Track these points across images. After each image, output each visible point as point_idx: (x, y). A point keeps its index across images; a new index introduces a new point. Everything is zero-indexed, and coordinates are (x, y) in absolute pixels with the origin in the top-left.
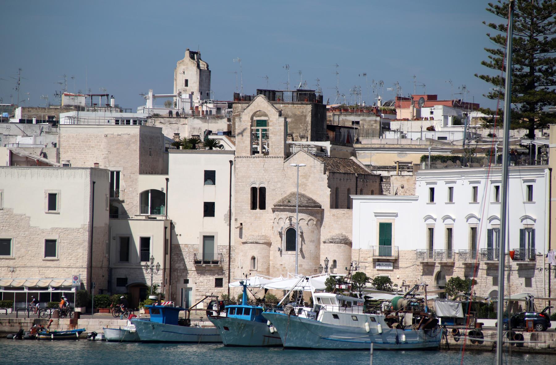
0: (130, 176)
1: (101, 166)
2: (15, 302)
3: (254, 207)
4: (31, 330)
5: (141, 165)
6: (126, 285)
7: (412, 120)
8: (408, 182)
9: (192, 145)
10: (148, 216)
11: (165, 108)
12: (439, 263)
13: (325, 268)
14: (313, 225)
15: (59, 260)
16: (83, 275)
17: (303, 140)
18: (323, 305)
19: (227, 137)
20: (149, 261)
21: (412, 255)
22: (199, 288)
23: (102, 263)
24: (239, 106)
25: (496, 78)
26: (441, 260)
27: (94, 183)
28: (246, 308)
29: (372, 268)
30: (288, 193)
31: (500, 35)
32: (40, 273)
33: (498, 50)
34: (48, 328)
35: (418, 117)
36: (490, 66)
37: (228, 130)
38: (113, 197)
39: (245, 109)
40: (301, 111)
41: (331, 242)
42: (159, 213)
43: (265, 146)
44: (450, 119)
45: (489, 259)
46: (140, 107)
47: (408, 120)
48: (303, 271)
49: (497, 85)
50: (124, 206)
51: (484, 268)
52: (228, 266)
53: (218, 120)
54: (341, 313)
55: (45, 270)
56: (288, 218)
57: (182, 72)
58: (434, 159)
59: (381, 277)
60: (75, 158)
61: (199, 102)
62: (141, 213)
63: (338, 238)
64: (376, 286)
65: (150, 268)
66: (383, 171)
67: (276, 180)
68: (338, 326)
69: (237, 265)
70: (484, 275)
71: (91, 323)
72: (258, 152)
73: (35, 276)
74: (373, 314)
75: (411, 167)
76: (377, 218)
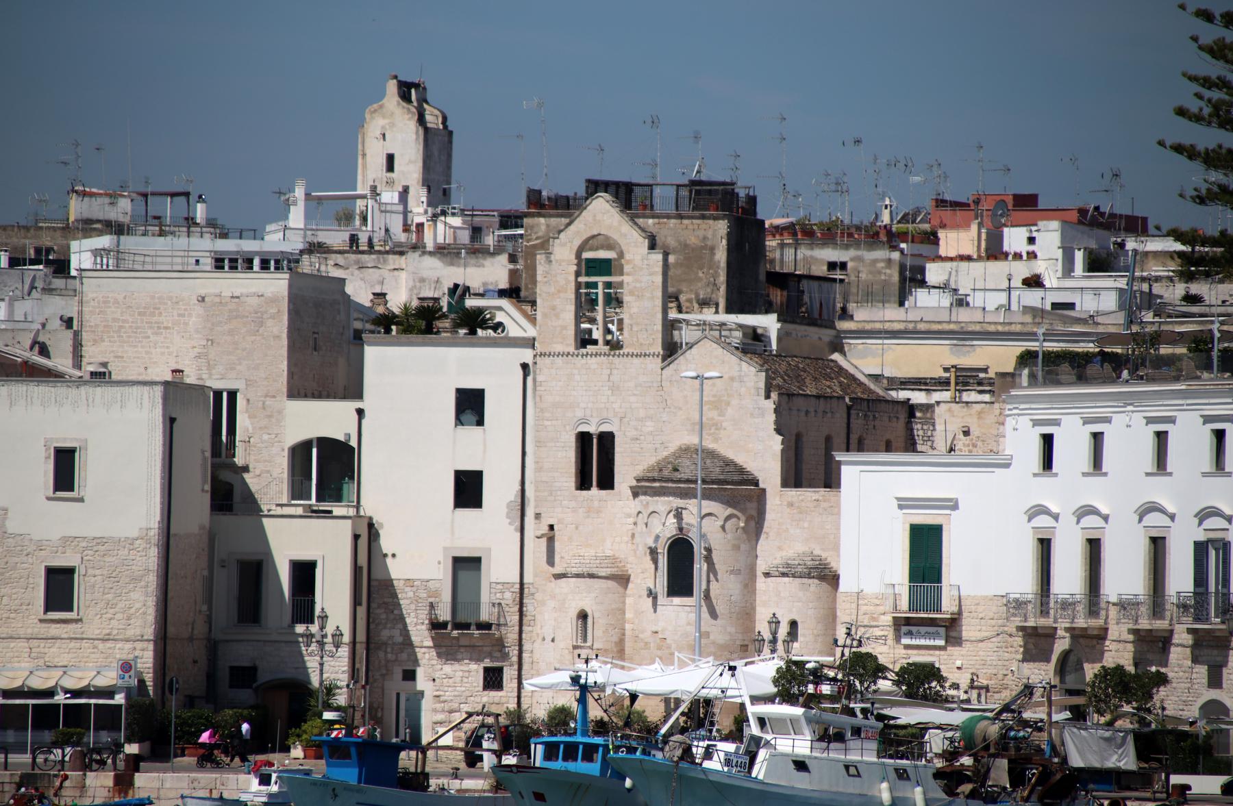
0: (264, 404)
1: (188, 376)
3: (583, 483)
4: (12, 801)
5: (291, 375)
6: (254, 685)
7: (980, 258)
8: (980, 418)
9: (423, 324)
10: (310, 506)
11: (338, 228)
12: (1067, 630)
13: (770, 642)
14: (737, 529)
15: (81, 620)
16: (143, 660)
17: (705, 310)
18: (768, 737)
19: (513, 304)
20: (312, 622)
21: (994, 609)
22: (442, 693)
23: (193, 629)
24: (541, 224)
25: (1213, 150)
26: (1072, 622)
27: (172, 420)
28: (586, 745)
29: (890, 642)
30: (673, 447)
31: (1224, 39)
32: (33, 655)
33: (1219, 78)
34: (56, 795)
35: (995, 251)
36: (1198, 118)
37: (511, 283)
38: (220, 456)
39: (560, 232)
40: (701, 237)
41: (784, 575)
42: (338, 498)
43: (610, 326)
44: (1079, 256)
45: (1197, 619)
46: (273, 225)
47: (968, 258)
48: (713, 650)
49: (1216, 167)
50: (248, 481)
51: (1185, 643)
52: (516, 636)
53: (485, 259)
54: (816, 758)
55: (44, 647)
56: (673, 513)
57: (378, 133)
58: (1053, 359)
59: (914, 664)
60: (123, 357)
61: (426, 212)
62: (293, 499)
63: (801, 562)
64: (904, 688)
65: (317, 642)
66: (913, 390)
67: (642, 413)
68: (806, 790)
69: (539, 632)
70: (1185, 661)
71: (167, 785)
72: (595, 342)
73: (19, 662)
74: (905, 762)
75: (986, 381)
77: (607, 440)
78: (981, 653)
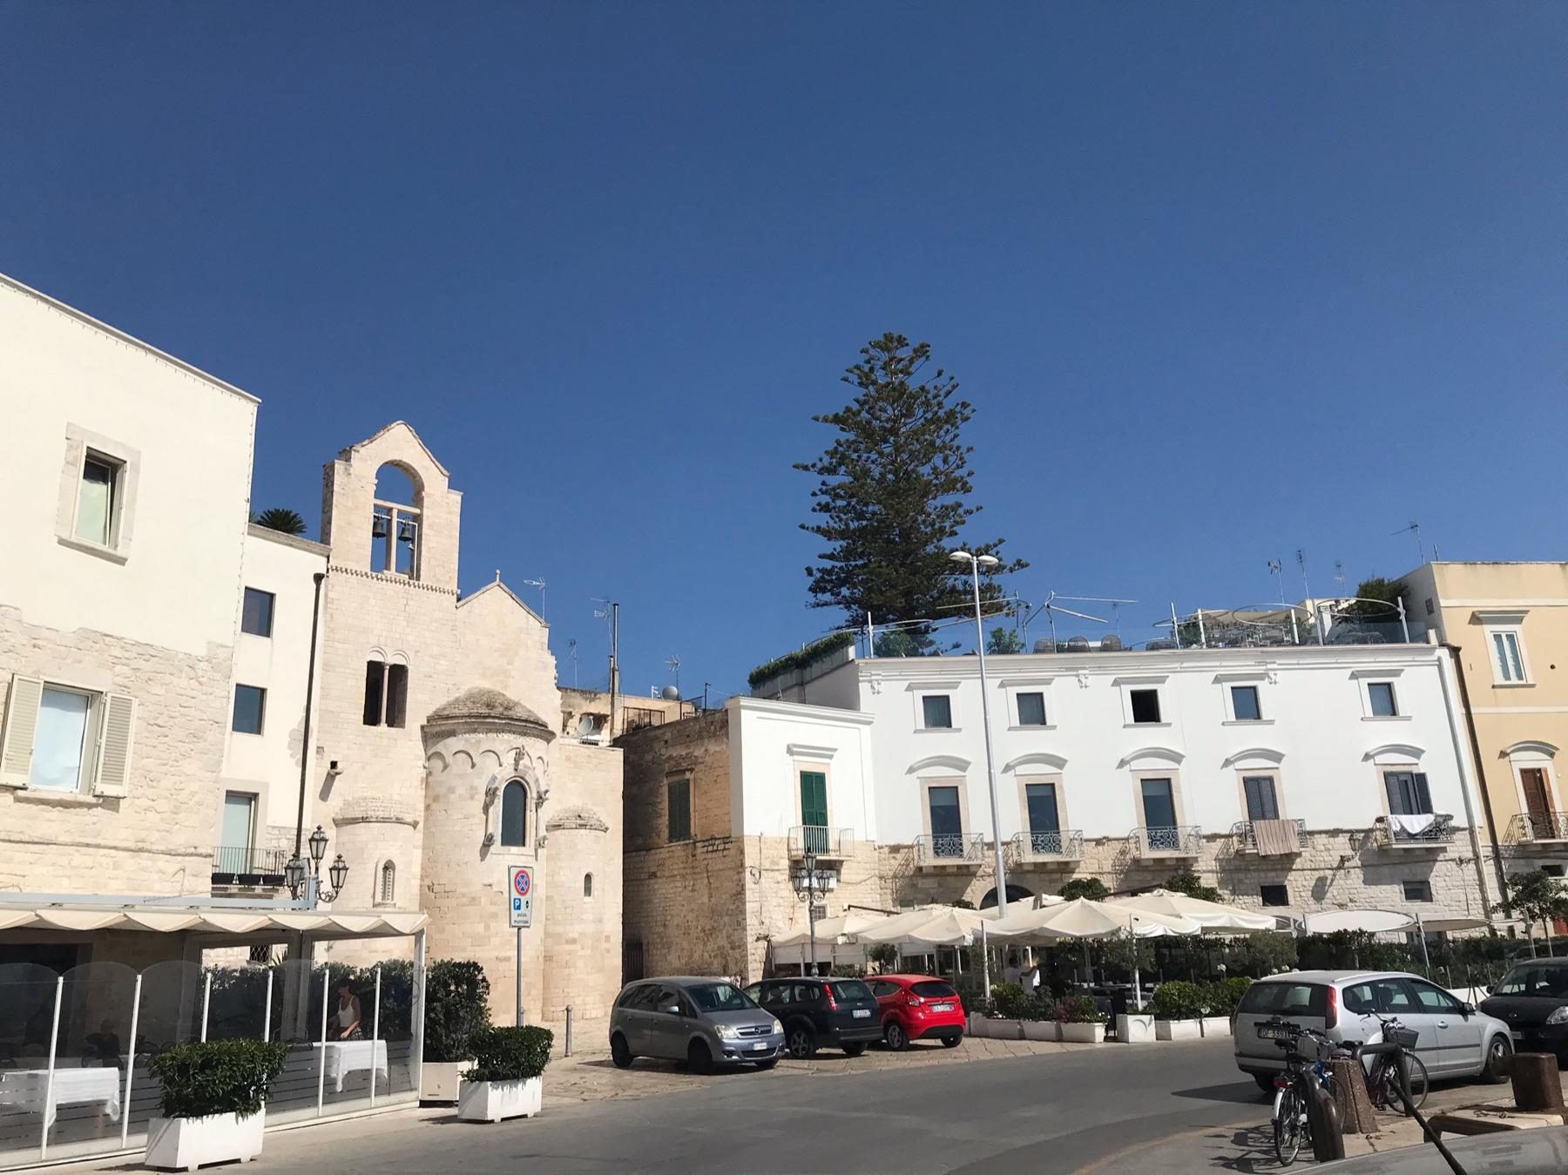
2: (57, 1055)
3: (371, 718)
76: (796, 757)
77: (399, 672)
78: (859, 895)
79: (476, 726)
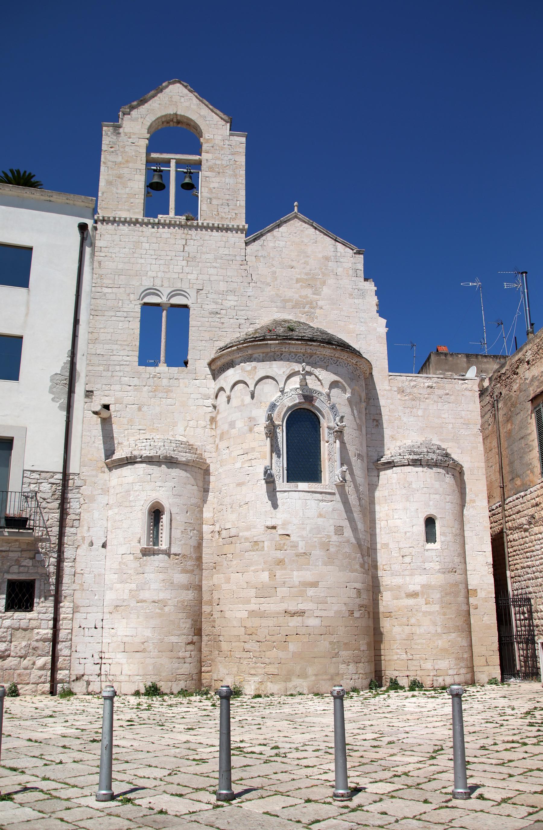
79: (250, 352)
